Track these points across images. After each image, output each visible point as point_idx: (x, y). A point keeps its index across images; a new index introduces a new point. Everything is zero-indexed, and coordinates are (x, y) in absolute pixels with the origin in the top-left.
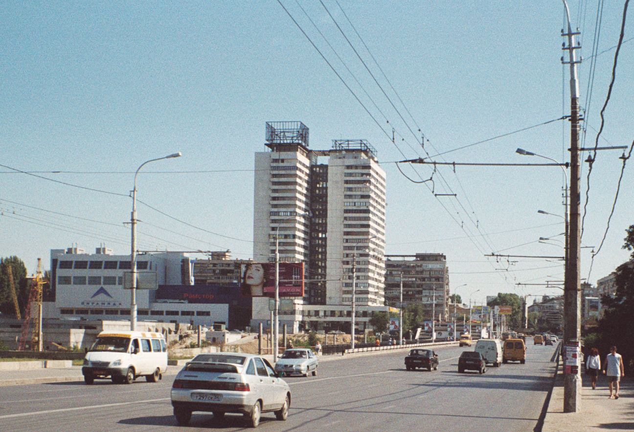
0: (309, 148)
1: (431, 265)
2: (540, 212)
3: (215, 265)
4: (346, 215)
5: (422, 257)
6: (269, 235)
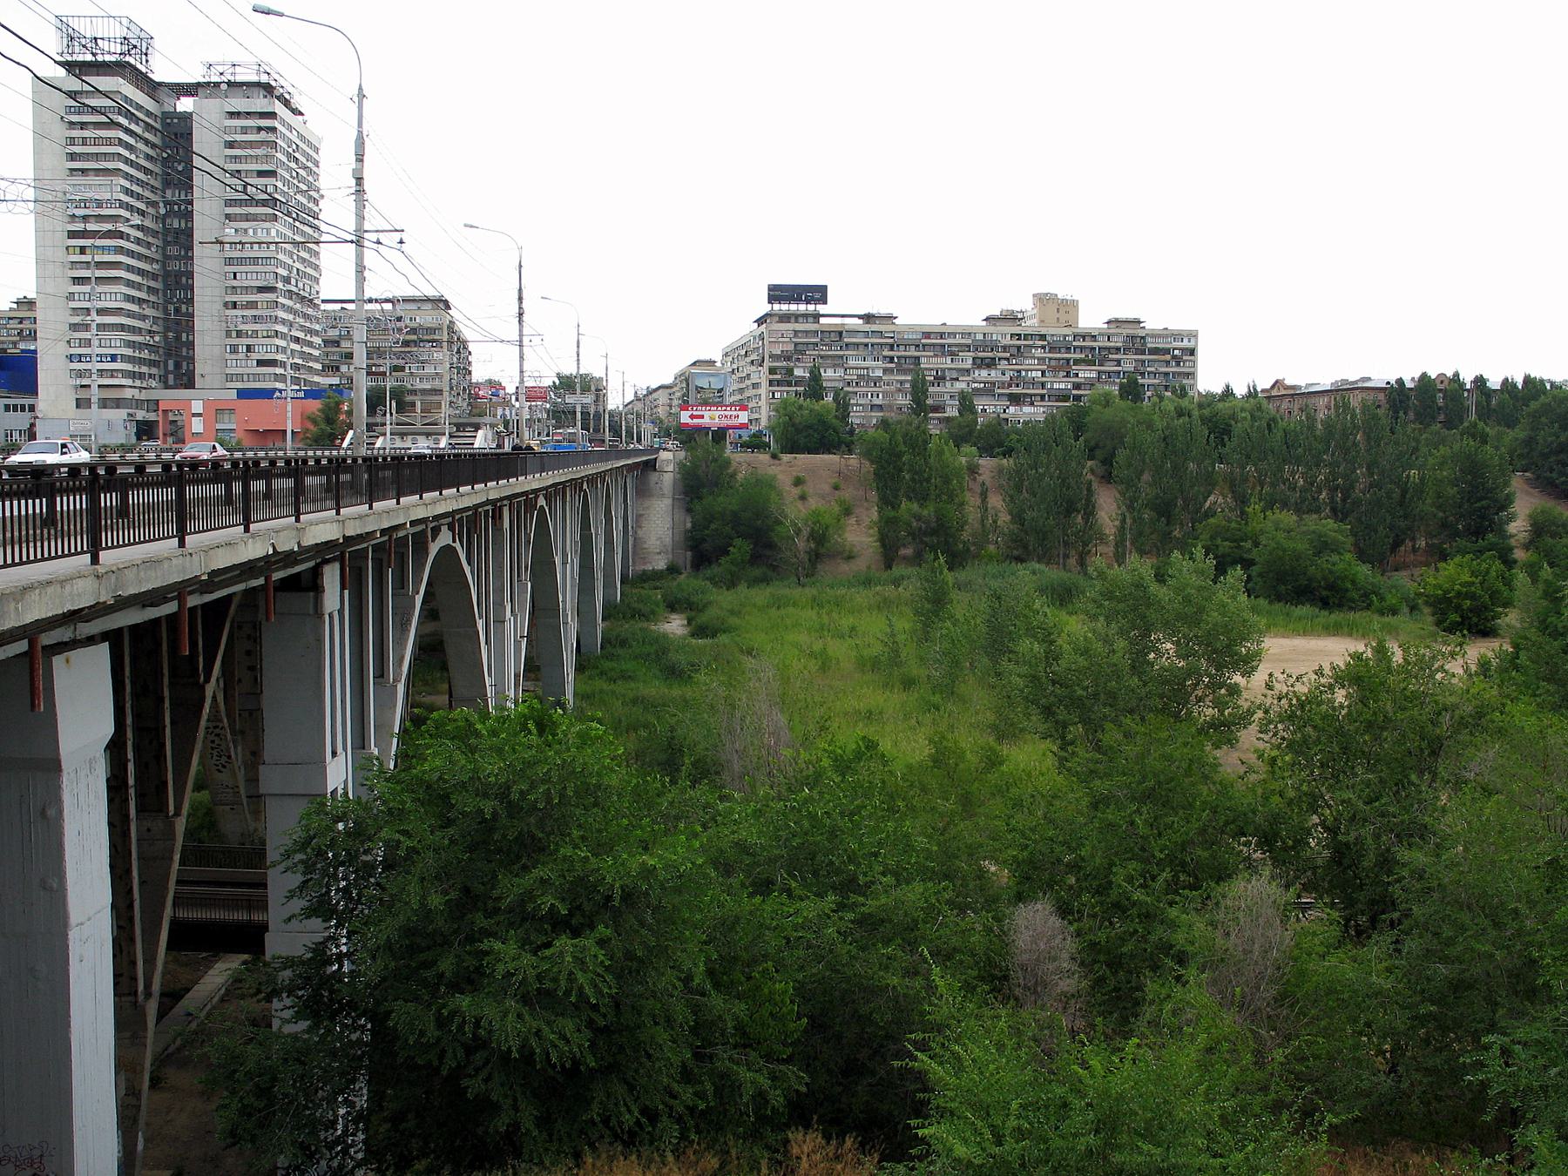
0: (157, 77)
1: (426, 318)
2: (466, 225)
3: (21, 320)
4: (229, 210)
5: (868, 318)
6: (67, 248)
